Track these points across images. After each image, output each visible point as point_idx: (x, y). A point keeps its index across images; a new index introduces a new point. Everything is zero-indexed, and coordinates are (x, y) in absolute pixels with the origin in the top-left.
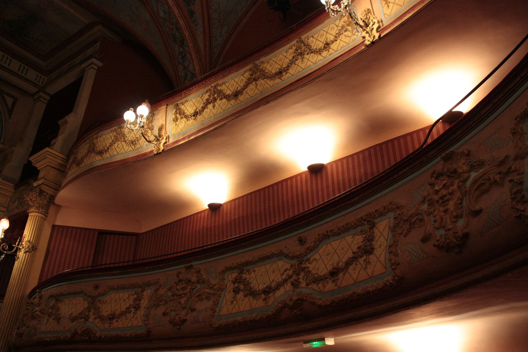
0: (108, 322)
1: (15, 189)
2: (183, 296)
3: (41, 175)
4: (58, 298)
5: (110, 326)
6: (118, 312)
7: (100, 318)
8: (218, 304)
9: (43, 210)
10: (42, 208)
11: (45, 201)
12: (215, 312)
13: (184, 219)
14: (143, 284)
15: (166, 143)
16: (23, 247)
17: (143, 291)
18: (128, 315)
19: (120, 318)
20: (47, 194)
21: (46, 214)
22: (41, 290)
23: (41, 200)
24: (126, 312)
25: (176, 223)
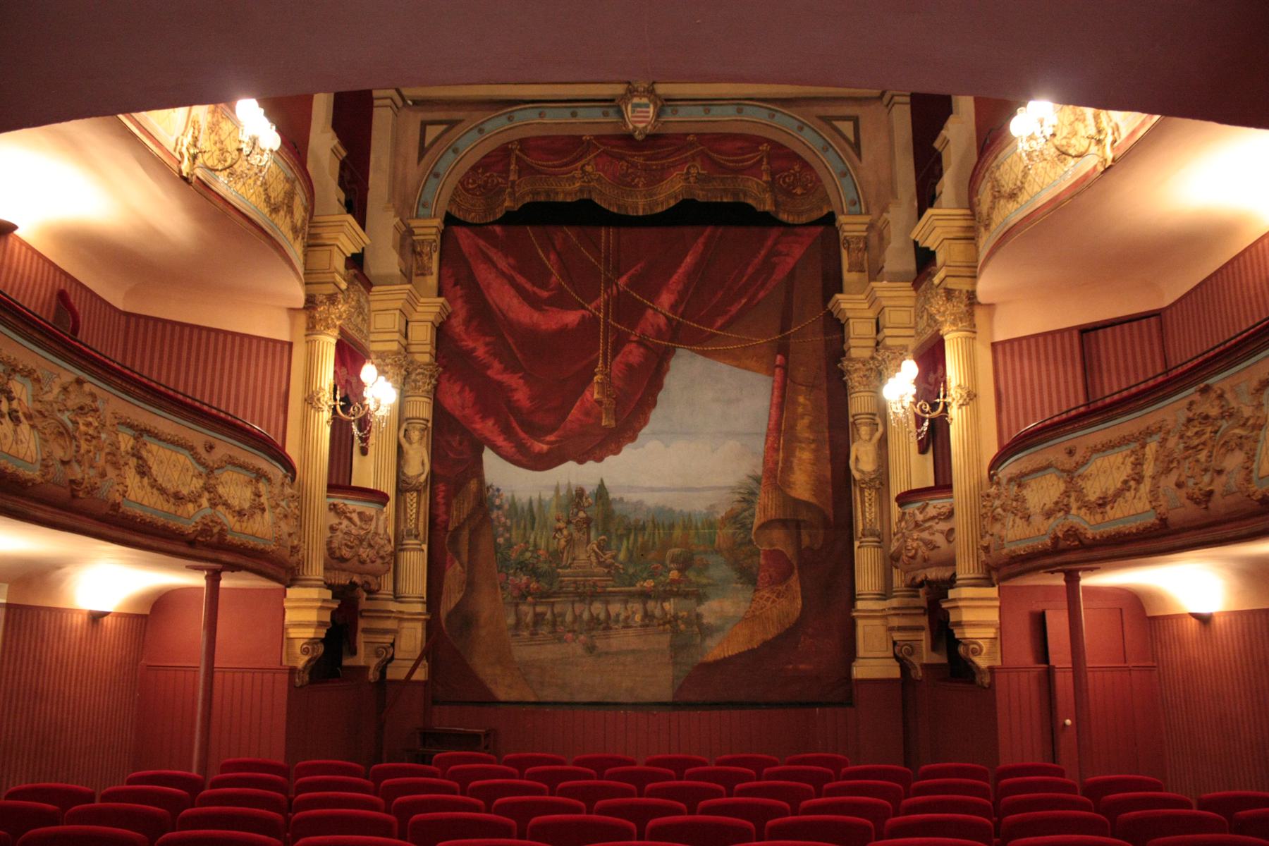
0: (1099, 511)
1: (916, 289)
2: (1200, 447)
3: (940, 259)
4: (1019, 480)
5: (1104, 518)
6: (1111, 492)
7: (1086, 506)
8: (1254, 455)
9: (964, 324)
10: (961, 320)
11: (962, 306)
12: (1251, 471)
13: (1236, 258)
14: (1140, 433)
15: (1115, 141)
16: (954, 399)
17: (1143, 447)
18: (1127, 494)
19: (1115, 502)
20: (961, 291)
21: (972, 328)
22: (997, 469)
23: (954, 306)
24: (1123, 490)
25: (1236, 262)
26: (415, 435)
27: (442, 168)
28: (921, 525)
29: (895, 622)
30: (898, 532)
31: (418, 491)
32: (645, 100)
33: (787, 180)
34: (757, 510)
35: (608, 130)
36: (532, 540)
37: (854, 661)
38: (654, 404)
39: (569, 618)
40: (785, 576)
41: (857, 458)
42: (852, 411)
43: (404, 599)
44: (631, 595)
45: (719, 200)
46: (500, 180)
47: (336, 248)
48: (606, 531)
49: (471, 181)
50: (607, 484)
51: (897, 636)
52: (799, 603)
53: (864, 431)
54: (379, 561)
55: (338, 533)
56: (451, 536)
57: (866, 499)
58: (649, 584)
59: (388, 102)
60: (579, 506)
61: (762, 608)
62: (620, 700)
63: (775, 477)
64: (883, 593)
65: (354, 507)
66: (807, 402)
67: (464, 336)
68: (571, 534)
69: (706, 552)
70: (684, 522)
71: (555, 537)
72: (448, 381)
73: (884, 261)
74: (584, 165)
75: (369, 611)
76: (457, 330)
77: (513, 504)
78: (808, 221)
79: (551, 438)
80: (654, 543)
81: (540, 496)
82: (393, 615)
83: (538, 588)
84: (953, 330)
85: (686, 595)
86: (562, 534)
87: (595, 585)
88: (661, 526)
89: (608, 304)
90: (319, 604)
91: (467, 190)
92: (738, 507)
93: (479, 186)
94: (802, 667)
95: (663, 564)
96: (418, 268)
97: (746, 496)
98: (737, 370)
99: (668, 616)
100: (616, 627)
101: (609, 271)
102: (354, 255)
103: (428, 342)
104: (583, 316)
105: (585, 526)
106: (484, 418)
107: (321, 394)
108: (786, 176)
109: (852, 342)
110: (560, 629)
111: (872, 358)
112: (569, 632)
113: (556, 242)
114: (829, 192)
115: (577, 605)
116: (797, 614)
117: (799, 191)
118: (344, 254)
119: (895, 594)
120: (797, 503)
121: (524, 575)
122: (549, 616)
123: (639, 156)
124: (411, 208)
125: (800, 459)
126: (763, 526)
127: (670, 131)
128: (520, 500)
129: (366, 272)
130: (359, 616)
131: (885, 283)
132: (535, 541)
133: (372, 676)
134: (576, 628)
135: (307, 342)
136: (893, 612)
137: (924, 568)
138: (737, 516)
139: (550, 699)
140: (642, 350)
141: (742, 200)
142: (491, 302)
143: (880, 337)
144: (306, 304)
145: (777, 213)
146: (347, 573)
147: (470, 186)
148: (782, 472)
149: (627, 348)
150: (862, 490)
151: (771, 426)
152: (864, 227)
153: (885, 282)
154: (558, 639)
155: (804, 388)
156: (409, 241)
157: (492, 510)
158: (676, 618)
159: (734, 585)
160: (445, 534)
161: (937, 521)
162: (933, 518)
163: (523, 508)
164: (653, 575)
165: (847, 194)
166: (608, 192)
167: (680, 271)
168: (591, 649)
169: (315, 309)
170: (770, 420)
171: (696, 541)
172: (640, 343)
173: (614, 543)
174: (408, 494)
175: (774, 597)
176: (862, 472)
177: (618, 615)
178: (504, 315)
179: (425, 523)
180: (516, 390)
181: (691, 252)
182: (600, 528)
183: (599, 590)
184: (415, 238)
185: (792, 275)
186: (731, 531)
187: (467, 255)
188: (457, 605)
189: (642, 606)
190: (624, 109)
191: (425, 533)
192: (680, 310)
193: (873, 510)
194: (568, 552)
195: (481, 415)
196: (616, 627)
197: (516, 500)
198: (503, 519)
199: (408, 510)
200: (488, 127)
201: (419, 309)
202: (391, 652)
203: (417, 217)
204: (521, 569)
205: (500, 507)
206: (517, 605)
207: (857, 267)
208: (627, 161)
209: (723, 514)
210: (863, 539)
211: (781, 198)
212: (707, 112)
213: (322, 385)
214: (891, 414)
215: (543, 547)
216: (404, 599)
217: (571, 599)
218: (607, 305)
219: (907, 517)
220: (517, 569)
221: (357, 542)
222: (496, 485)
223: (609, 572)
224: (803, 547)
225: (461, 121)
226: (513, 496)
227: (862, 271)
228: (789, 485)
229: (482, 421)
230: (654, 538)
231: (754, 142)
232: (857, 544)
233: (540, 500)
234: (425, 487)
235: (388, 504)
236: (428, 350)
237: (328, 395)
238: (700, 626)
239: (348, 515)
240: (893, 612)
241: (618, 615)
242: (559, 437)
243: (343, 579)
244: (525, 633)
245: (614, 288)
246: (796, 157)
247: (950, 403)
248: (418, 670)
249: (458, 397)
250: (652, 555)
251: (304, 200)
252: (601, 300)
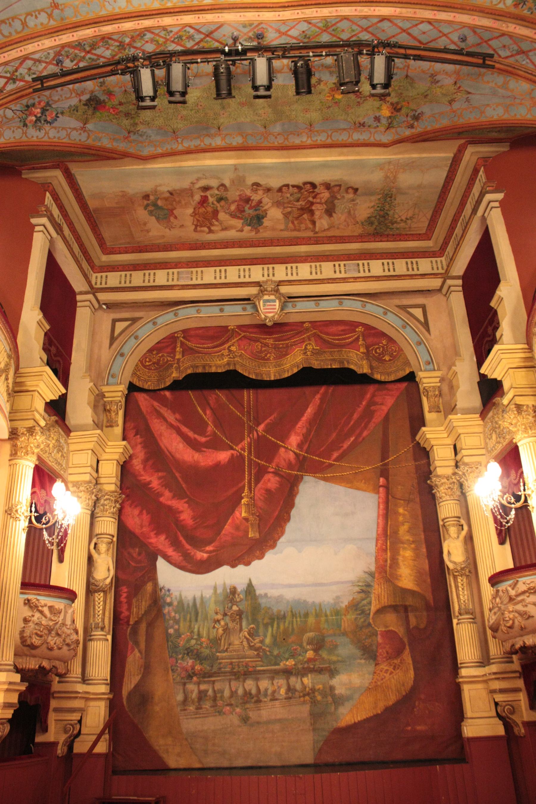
3: (506, 385)
9: (533, 431)
11: (530, 418)
20: (528, 406)
26: (103, 547)
27: (126, 350)
28: (514, 599)
29: (497, 685)
30: (493, 607)
31: (105, 592)
32: (272, 297)
33: (378, 351)
34: (373, 599)
35: (247, 321)
36: (196, 630)
37: (463, 721)
38: (288, 519)
39: (227, 693)
40: (399, 652)
41: (449, 553)
42: (441, 516)
43: (90, 682)
44: (276, 673)
45: (329, 367)
46: (169, 359)
47: (36, 393)
48: (254, 621)
49: (147, 360)
50: (254, 583)
51: (499, 698)
52: (411, 674)
53: (453, 531)
54: (65, 648)
55: (31, 624)
56: (132, 628)
57: (460, 585)
58: (290, 663)
59: (88, 303)
60: (233, 601)
61: (382, 679)
62: (271, 764)
63: (386, 572)
64: (481, 661)
65: (45, 602)
66: (406, 512)
67: (143, 473)
68: (227, 624)
69: (335, 635)
70: (316, 610)
71: (214, 627)
72: (130, 507)
73: (456, 401)
74: (230, 347)
75: (59, 692)
76: (137, 468)
77: (181, 602)
78: (396, 378)
79: (209, 548)
80: (293, 629)
81: (202, 595)
82: (80, 695)
83: (201, 670)
84: (525, 437)
85: (320, 671)
86: (220, 624)
87: (247, 665)
88: (298, 615)
89: (251, 445)
90: (6, 687)
91: (145, 366)
92: (358, 597)
93: (154, 363)
94: (419, 728)
95: (301, 646)
96: (108, 421)
97: (364, 588)
98: (350, 490)
99: (307, 689)
100: (266, 700)
101: (250, 421)
102: (52, 401)
103: (114, 475)
104: (232, 455)
105: (238, 617)
106: (157, 534)
107: (18, 507)
108: (377, 348)
109: (437, 463)
110: (220, 703)
111: (455, 474)
112: (227, 705)
113: (211, 402)
114: (409, 358)
115: (233, 683)
116: (411, 683)
117: (387, 358)
118: (45, 400)
119: (492, 661)
120: (404, 591)
121: (191, 659)
122: (210, 693)
123: (269, 338)
124: (103, 379)
125: (404, 557)
126: (380, 611)
127: (291, 321)
128: (186, 597)
129: (67, 423)
130: (51, 696)
131: (459, 416)
132: (199, 631)
133: (60, 750)
134: (233, 702)
135: (10, 465)
136: (493, 677)
137: (522, 636)
138: (358, 604)
139: (212, 765)
140: (277, 478)
141: (346, 366)
142: (163, 447)
143: (459, 457)
144: (10, 435)
145: (372, 373)
146: (37, 659)
147: (147, 364)
148: (390, 567)
149: (267, 477)
150: (455, 577)
151: (379, 532)
152: (438, 380)
153: (459, 415)
154: (218, 712)
155: (402, 502)
156: (102, 402)
157: (164, 606)
158: (313, 690)
159: (359, 661)
160: (128, 628)
161: (528, 594)
162: (524, 593)
163: (188, 604)
164: (293, 656)
165: (423, 357)
166: (248, 365)
167: (304, 419)
168: (245, 720)
169: (17, 439)
170: (378, 528)
171: (326, 626)
172: (276, 473)
173: (261, 630)
174: (96, 594)
175: (391, 669)
176: (455, 563)
177: (266, 690)
178: (173, 456)
179: (110, 618)
180: (182, 512)
181: (311, 405)
182: (250, 618)
183: (251, 669)
184: (105, 399)
185: (386, 418)
186: (353, 617)
187: (145, 412)
188: (137, 686)
189: (285, 681)
190: (258, 304)
191: (109, 627)
192: (305, 448)
193: (466, 593)
194: (225, 639)
195: (155, 532)
196: (266, 700)
197: (183, 598)
198: (173, 614)
199: (97, 607)
200: (160, 321)
201: (107, 450)
202: (78, 729)
203: (107, 384)
204: (188, 654)
205: (170, 604)
206: (185, 684)
207: (435, 409)
208: (261, 343)
209: (347, 604)
210: (460, 617)
211: (375, 364)
212: (317, 305)
213: (20, 500)
214: (483, 506)
215: (205, 635)
216: (90, 682)
217: (228, 677)
218: (250, 445)
219: (501, 593)
220: (184, 654)
221: (46, 632)
222: (167, 587)
223: (258, 654)
224: (411, 627)
225: (141, 318)
226: (180, 595)
227: (439, 412)
228: (397, 577)
229: (157, 537)
230: (293, 626)
231: (352, 325)
232: (455, 621)
233: (202, 598)
234: (110, 588)
235: (76, 601)
236: (114, 482)
237: (24, 508)
238: (333, 696)
239: (40, 608)
240: (493, 677)
241: (266, 690)
243: (32, 664)
244: (191, 708)
245: (255, 433)
246: (383, 335)
247: (529, 495)
248: (100, 744)
249: (137, 518)
250: (292, 638)
251: (8, 349)
252: (247, 441)
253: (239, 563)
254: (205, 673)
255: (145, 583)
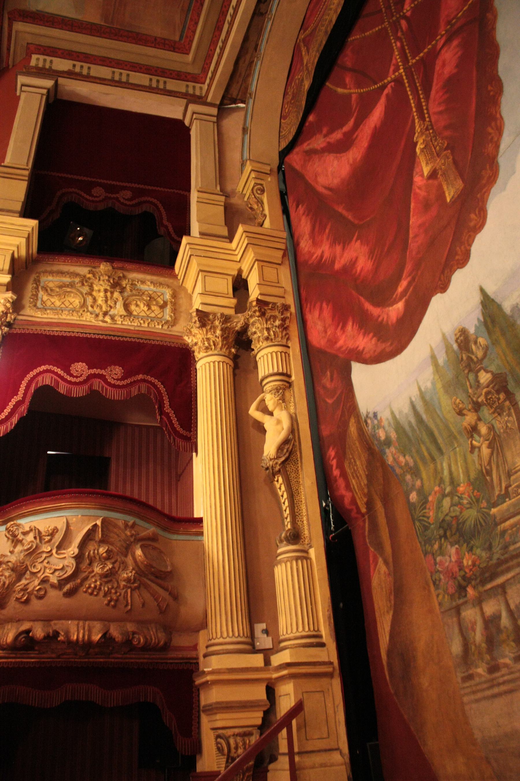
50: (490, 290)
71: (473, 448)
86: (480, 435)
121: (452, 545)
132: (451, 473)
163: (410, 423)
194: (498, 467)
222: (371, 410)
233: (422, 395)
242: (409, 276)
253: (452, 272)
254: (483, 571)
255: (345, 424)
